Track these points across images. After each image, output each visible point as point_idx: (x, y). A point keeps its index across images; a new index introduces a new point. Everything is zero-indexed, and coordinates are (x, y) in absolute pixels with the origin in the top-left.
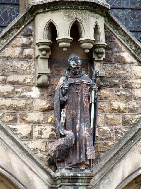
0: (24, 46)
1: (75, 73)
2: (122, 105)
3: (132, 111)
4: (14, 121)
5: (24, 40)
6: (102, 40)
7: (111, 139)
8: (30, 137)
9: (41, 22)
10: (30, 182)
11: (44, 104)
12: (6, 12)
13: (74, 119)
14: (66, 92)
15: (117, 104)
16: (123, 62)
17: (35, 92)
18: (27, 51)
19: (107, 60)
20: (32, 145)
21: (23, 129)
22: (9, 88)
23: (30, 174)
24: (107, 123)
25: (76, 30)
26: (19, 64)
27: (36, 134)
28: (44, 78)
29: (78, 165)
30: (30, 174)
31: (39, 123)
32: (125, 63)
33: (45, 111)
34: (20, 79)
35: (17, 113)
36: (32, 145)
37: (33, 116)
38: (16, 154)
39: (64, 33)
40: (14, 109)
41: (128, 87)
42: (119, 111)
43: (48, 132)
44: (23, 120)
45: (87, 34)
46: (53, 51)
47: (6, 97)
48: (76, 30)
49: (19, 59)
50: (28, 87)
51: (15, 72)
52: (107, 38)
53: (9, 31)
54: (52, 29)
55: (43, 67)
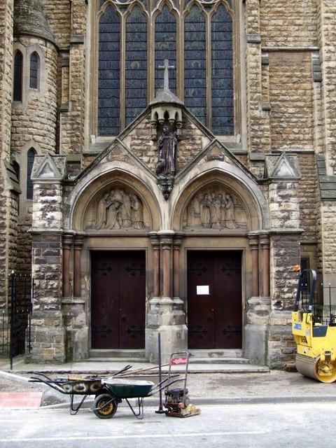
0: (147, 123)
1: (166, 134)
2: (190, 147)
3: (195, 150)
4: (142, 156)
5: (147, 121)
6: (180, 119)
7: (185, 162)
8: (149, 162)
9: (153, 111)
10: (148, 182)
11: (155, 148)
12: (221, 7)
13: (166, 154)
14: (162, 142)
15: (188, 147)
16: (191, 128)
17: (151, 143)
18: (148, 125)
19: (184, 128)
20: (149, 166)
21: (145, 159)
22: (140, 141)
23: (148, 178)
24: (184, 156)
25: (166, 115)
26: (144, 131)
27: (151, 161)
28: (154, 137)
29: (167, 174)
30: (148, 178)
31: (153, 156)
32: (192, 129)
33: (156, 151)
34: (145, 137)
35: (143, 152)
36: (149, 166)
37: (150, 153)
38: (195, 373)
39: (161, 117)
40: (142, 151)
41: (193, 139)
42: (189, 150)
43: (156, 160)
44: (146, 155)
45: (172, 116)
46: (158, 125)
47: (138, 146)
48: (166, 115)
49: (144, 129)
50: (148, 141)
51: (143, 134)
52: (183, 118)
53: (141, 116)
54: (156, 114)
55: (154, 132)
